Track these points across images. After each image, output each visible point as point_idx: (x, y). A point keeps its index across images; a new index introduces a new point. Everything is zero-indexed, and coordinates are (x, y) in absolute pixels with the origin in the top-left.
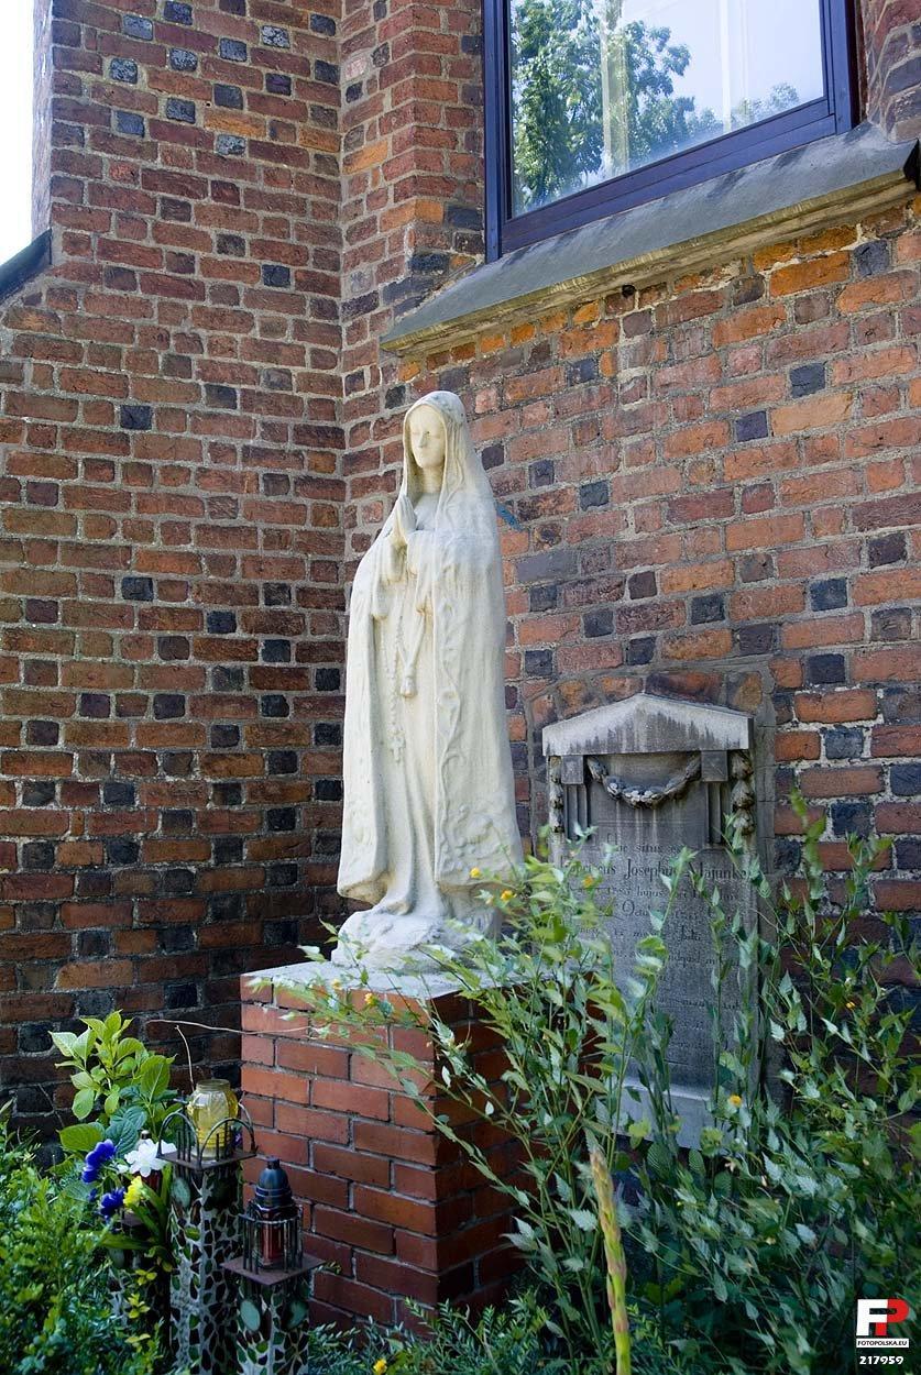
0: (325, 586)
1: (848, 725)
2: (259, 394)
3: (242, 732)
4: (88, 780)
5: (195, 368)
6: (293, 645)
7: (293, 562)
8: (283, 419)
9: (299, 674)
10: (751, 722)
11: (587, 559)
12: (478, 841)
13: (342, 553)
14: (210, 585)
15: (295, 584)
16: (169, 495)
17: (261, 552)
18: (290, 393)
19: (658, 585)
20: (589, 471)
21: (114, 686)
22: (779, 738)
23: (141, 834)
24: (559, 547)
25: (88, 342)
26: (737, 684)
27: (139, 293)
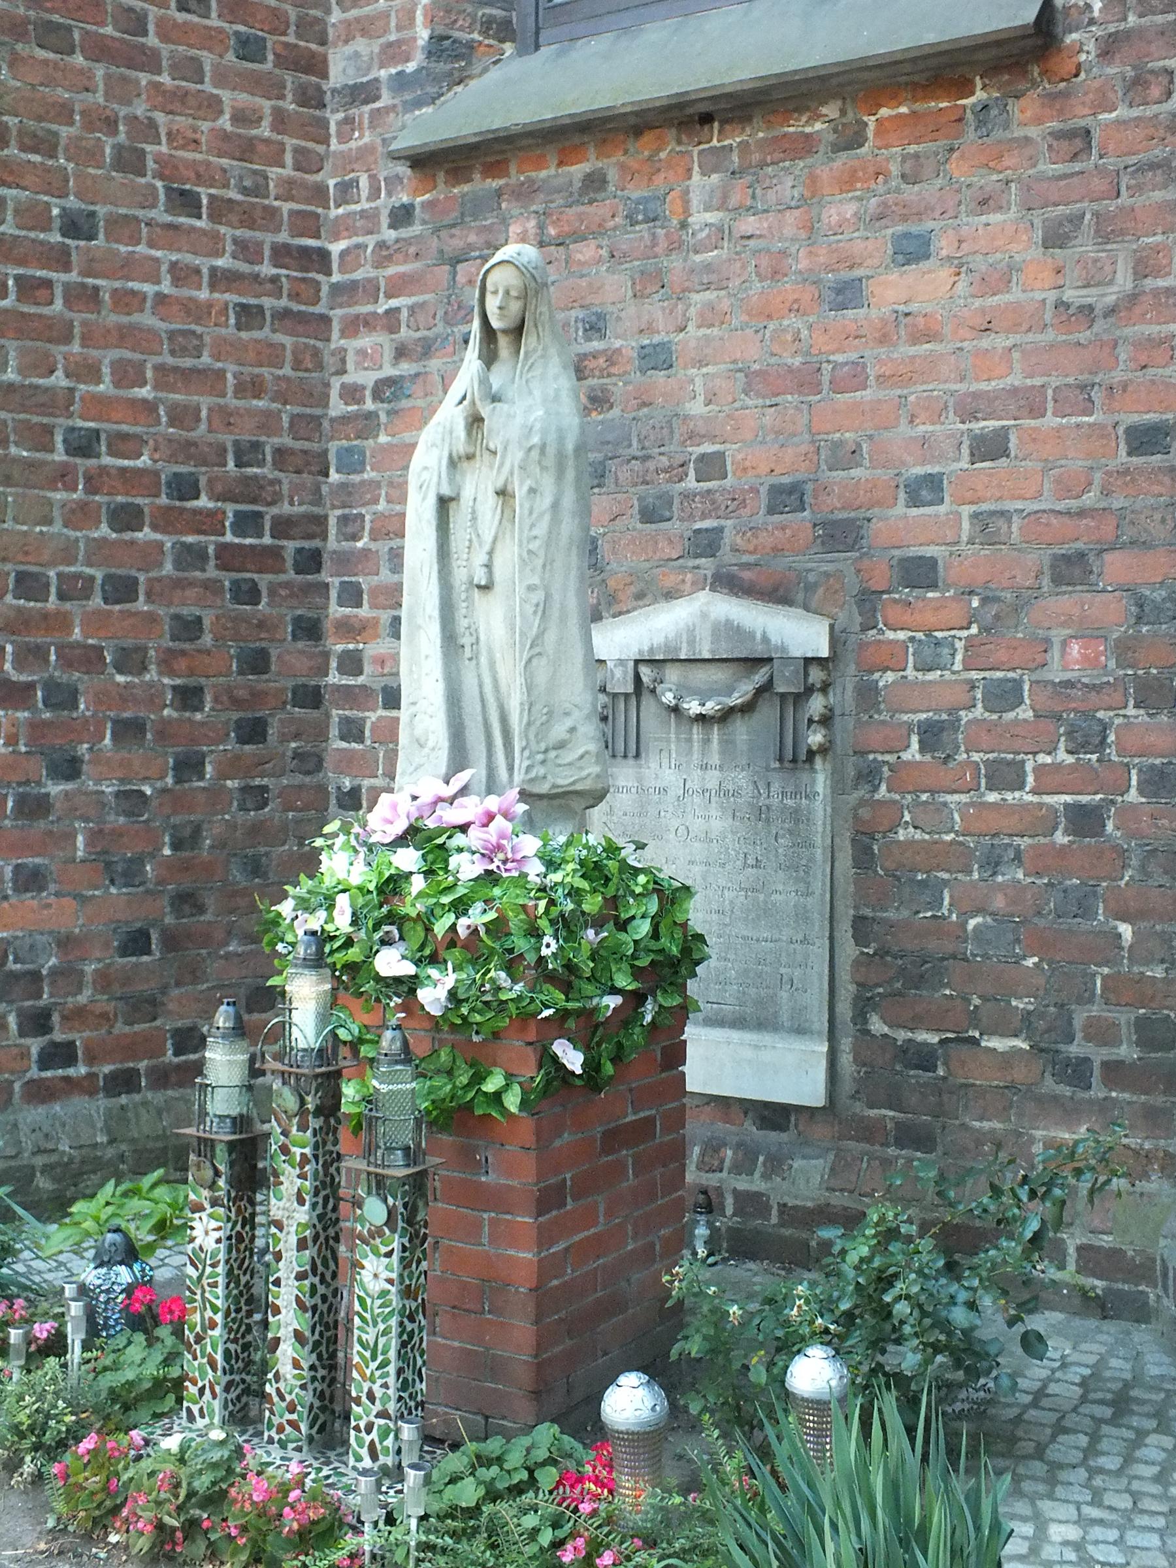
0: (306, 445)
1: (939, 634)
2: (230, 201)
3: (207, 623)
4: (23, 678)
5: (151, 164)
6: (268, 517)
7: (268, 414)
8: (258, 235)
9: (275, 553)
10: (832, 627)
11: (644, 433)
12: (561, 745)
13: (326, 406)
14: (170, 441)
15: (271, 443)
16: (120, 328)
17: (231, 401)
18: (266, 202)
19: (729, 468)
20: (648, 329)
21: (52, 564)
22: (863, 646)
23: (86, 746)
24: (610, 415)
25: (17, 120)
26: (816, 585)
27: (79, 59)
